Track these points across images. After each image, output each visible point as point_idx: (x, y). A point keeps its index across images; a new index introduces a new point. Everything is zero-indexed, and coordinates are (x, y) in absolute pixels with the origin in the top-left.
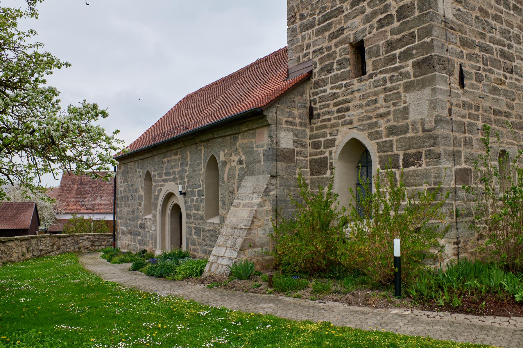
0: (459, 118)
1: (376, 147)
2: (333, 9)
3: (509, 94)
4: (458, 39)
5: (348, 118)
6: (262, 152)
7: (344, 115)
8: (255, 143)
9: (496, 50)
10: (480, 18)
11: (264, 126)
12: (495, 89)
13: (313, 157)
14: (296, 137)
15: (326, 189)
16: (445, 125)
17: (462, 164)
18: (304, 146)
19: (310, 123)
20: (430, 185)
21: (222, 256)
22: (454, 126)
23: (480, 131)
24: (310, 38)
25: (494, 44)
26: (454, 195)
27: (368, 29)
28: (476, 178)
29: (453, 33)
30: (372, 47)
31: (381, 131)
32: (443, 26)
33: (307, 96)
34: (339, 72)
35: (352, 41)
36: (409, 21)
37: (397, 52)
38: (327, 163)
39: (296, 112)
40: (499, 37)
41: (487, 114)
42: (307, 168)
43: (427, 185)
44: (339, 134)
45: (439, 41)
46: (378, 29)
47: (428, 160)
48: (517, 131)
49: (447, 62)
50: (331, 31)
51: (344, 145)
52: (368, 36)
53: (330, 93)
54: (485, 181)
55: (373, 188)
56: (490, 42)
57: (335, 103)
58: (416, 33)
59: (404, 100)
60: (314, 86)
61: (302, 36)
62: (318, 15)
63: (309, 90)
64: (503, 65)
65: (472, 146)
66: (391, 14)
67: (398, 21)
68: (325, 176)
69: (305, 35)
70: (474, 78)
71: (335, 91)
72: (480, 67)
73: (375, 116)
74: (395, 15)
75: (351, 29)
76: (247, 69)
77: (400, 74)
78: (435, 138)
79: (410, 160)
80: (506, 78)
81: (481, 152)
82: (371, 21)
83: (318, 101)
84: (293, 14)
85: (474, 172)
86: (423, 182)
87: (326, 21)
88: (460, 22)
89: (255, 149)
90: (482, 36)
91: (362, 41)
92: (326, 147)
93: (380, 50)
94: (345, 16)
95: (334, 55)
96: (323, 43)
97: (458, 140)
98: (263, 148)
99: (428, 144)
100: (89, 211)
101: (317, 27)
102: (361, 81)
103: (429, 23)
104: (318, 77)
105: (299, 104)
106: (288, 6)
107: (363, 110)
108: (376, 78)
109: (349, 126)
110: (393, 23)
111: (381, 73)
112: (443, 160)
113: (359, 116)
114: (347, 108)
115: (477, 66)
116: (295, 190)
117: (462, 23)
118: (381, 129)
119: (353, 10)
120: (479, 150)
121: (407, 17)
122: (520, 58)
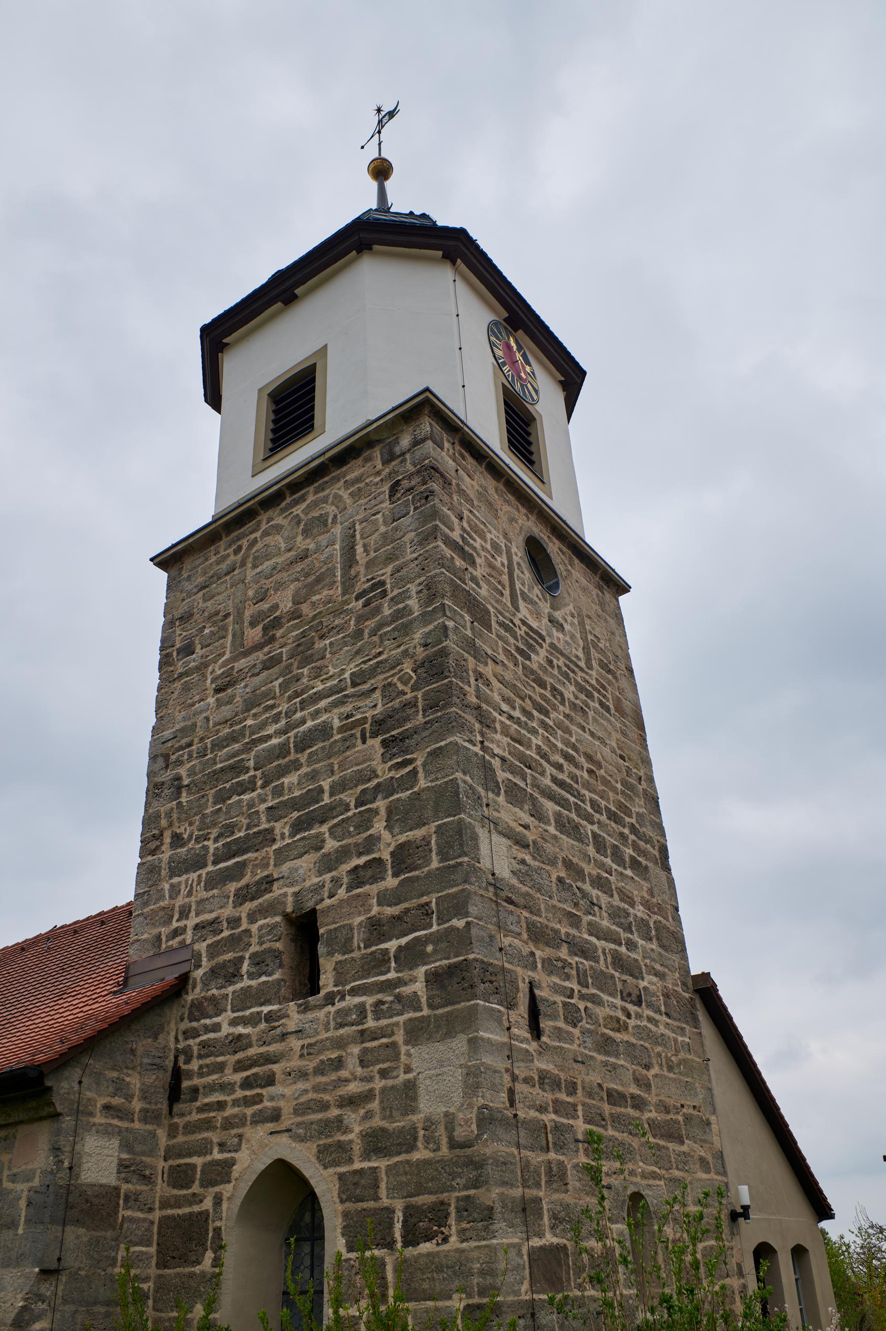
0: (533, 1114)
1: (338, 1186)
2: (251, 832)
3: (638, 1053)
4: (524, 925)
5: (268, 1104)
6: (25, 1193)
7: (260, 1096)
8: (9, 1169)
9: (604, 953)
10: (568, 881)
11: (41, 1119)
12: (608, 1040)
13: (170, 1212)
14: (128, 1153)
15: (199, 1310)
16: (500, 1131)
17: (544, 1235)
18: (147, 1179)
19: (170, 1113)
20: (470, 1296)
22: (522, 1133)
23: (580, 1145)
24: (190, 893)
25: (598, 938)
26: (530, 1322)
27: (328, 885)
28: (580, 1270)
29: (512, 911)
30: (335, 929)
31: (351, 1141)
32: (491, 895)
33: (169, 1040)
34: (253, 983)
35: (289, 909)
36: (418, 877)
37: (392, 945)
38: (207, 1230)
39: (135, 1081)
40: (608, 924)
41: (594, 1102)
42: (149, 1245)
43: (464, 1296)
44: (244, 1146)
45: (482, 928)
46: (350, 889)
47: (464, 1225)
48: (662, 1143)
49: (500, 977)
50: (243, 882)
51: (254, 1177)
52: (328, 902)
53: (229, 1035)
54: (600, 1281)
55: (325, 1307)
56: (591, 934)
57: (239, 1062)
58: (433, 905)
59: (406, 1064)
60: (190, 1013)
61: (172, 885)
62: (216, 840)
63: (176, 1024)
64: (619, 986)
65: (566, 1184)
66: (380, 858)
67: (395, 875)
68: (197, 1269)
69: (180, 883)
70: (561, 1014)
71: (241, 1030)
72: (572, 990)
73: (337, 1100)
74: (390, 861)
75: (289, 881)
76: (23, 949)
77: (399, 998)
78: (478, 1165)
79: (421, 1224)
80: (629, 1016)
81: (588, 1199)
82: (336, 869)
83: (195, 1053)
84: (156, 832)
85: (573, 1254)
86: (453, 1287)
87: (234, 856)
88: (527, 889)
89: (7, 1184)
90: (574, 920)
91: (314, 911)
92: (207, 1183)
93: (353, 937)
94: (278, 852)
95: (246, 939)
96: (221, 907)
97: (532, 1169)
98: (30, 1184)
99: (462, 1181)
101: (210, 868)
102: (305, 1009)
103: (460, 887)
104: (202, 990)
105: (146, 1060)
106: (146, 811)
107: (307, 1085)
108: (343, 1004)
109: (270, 1126)
110: (383, 879)
111: (354, 992)
112: (499, 1225)
113: (296, 1099)
114: (269, 1076)
115: (565, 988)
116: (107, 1315)
117: (530, 890)
118: (351, 1136)
119: (295, 839)
120: (582, 1194)
121: (415, 869)
122: (653, 972)
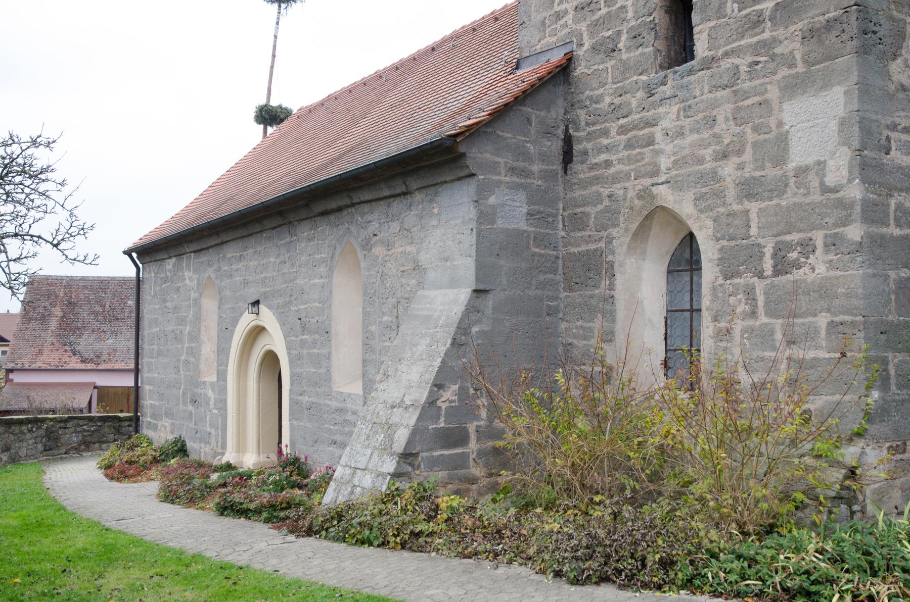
21: (364, 468)
76: (433, 49)
100: (90, 366)
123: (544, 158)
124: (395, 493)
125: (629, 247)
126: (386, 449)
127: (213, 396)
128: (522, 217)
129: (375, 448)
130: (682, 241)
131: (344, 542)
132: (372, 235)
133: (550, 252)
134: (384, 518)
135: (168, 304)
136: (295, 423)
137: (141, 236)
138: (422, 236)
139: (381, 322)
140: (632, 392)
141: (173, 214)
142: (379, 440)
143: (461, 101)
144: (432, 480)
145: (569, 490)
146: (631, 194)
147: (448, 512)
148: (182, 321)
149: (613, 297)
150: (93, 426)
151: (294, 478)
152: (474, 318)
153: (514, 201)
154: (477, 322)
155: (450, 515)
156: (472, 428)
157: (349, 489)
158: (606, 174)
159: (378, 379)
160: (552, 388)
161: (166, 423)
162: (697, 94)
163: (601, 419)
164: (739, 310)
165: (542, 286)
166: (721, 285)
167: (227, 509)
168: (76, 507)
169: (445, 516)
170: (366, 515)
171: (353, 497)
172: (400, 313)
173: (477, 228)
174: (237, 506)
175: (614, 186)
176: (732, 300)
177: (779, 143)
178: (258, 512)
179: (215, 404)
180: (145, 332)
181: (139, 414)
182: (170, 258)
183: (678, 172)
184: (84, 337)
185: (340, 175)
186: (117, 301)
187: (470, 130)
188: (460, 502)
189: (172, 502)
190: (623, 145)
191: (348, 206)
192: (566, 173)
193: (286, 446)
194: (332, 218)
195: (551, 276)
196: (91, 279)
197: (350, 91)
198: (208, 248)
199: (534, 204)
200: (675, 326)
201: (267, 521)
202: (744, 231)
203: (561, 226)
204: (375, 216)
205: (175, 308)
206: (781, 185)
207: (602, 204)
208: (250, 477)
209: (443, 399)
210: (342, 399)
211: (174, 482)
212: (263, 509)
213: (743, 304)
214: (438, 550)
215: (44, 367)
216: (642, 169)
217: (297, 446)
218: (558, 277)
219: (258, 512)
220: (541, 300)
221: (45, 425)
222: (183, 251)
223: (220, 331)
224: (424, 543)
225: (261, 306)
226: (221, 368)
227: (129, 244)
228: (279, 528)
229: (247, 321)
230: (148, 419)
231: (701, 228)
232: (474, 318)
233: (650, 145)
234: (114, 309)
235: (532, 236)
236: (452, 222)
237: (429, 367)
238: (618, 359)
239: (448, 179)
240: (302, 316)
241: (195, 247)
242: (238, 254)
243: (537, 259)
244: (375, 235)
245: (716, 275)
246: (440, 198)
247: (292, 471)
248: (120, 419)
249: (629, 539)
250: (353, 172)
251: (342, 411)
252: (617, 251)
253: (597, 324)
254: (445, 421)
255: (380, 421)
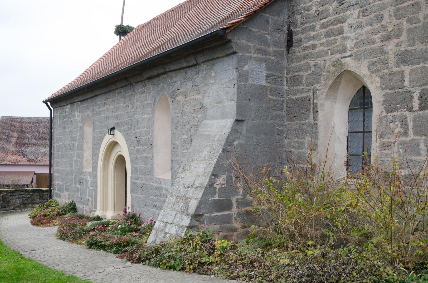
21: (171, 222)
100: (32, 163)
123: (276, 44)
124: (190, 237)
125: (327, 95)
126: (184, 211)
127: (90, 180)
128: (263, 78)
129: (178, 211)
130: (358, 91)
131: (159, 267)
132: (176, 90)
133: (279, 99)
134: (183, 253)
135: (66, 130)
136: (134, 195)
137: (53, 93)
138: (205, 89)
139: (181, 139)
140: (330, 180)
141: (70, 82)
142: (180, 207)
143: (227, 13)
144: (211, 230)
145: (292, 236)
146: (328, 63)
147: (221, 250)
148: (74, 139)
149: (316, 124)
150: (28, 195)
151: (132, 226)
152: (235, 136)
153: (259, 68)
154: (237, 138)
155: (222, 252)
156: (234, 200)
157: (163, 235)
158: (313, 52)
159: (179, 171)
160: (281, 177)
161: (66, 193)
162: (371, 2)
163: (311, 196)
164: (396, 131)
165: (274, 118)
166: (385, 117)
167: (92, 245)
168: (9, 242)
169: (219, 253)
170: (172, 251)
171: (165, 240)
172: (192, 134)
173: (238, 84)
174: (99, 243)
175: (318, 59)
176: (392, 125)
177: (425, 29)
178: (111, 247)
179: (91, 184)
180: (55, 145)
181: (52, 189)
182: (68, 105)
183: (358, 50)
184: (29, 148)
185: (158, 55)
186: (46, 130)
187: (234, 25)
188: (228, 244)
189: (64, 240)
190: (323, 35)
191: (163, 74)
192: (288, 52)
193: (129, 208)
194: (154, 80)
195: (280, 112)
196: (32, 118)
197: (165, 15)
198: (87, 99)
199: (270, 71)
200: (353, 141)
201: (115, 252)
202: (400, 83)
203: (285, 83)
204: (178, 79)
205: (70, 132)
206: (425, 55)
207: (310, 70)
208: (108, 225)
209: (217, 183)
210: (160, 182)
211: (65, 228)
212: (113, 246)
213: (399, 128)
214: (215, 273)
215: (8, 163)
216: (336, 48)
217: (135, 207)
218: (283, 113)
219: (111, 247)
220: (274, 126)
221: (2, 194)
222: (74, 101)
223: (93, 144)
224: (207, 269)
225: (115, 130)
226: (94, 164)
227: (46, 98)
228: (122, 257)
229: (108, 139)
230: (57, 192)
231: (372, 82)
232: (235, 136)
233: (340, 34)
234: (44, 134)
235: (269, 89)
236: (223, 81)
237: (209, 164)
238: (320, 160)
239: (220, 56)
240: (138, 135)
241: (80, 98)
242: (103, 102)
243: (271, 102)
244: (178, 89)
245: (382, 110)
246: (216, 67)
247: (132, 222)
248: (42, 191)
249: (335, 272)
250: (166, 53)
251: (159, 188)
252: (319, 97)
253: (308, 139)
254: (218, 196)
255: (180, 196)
